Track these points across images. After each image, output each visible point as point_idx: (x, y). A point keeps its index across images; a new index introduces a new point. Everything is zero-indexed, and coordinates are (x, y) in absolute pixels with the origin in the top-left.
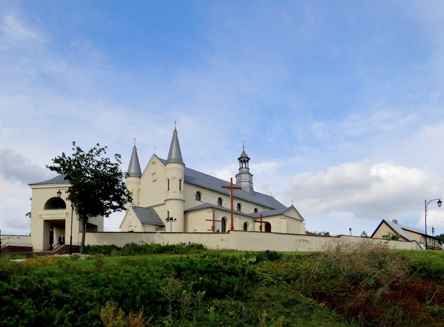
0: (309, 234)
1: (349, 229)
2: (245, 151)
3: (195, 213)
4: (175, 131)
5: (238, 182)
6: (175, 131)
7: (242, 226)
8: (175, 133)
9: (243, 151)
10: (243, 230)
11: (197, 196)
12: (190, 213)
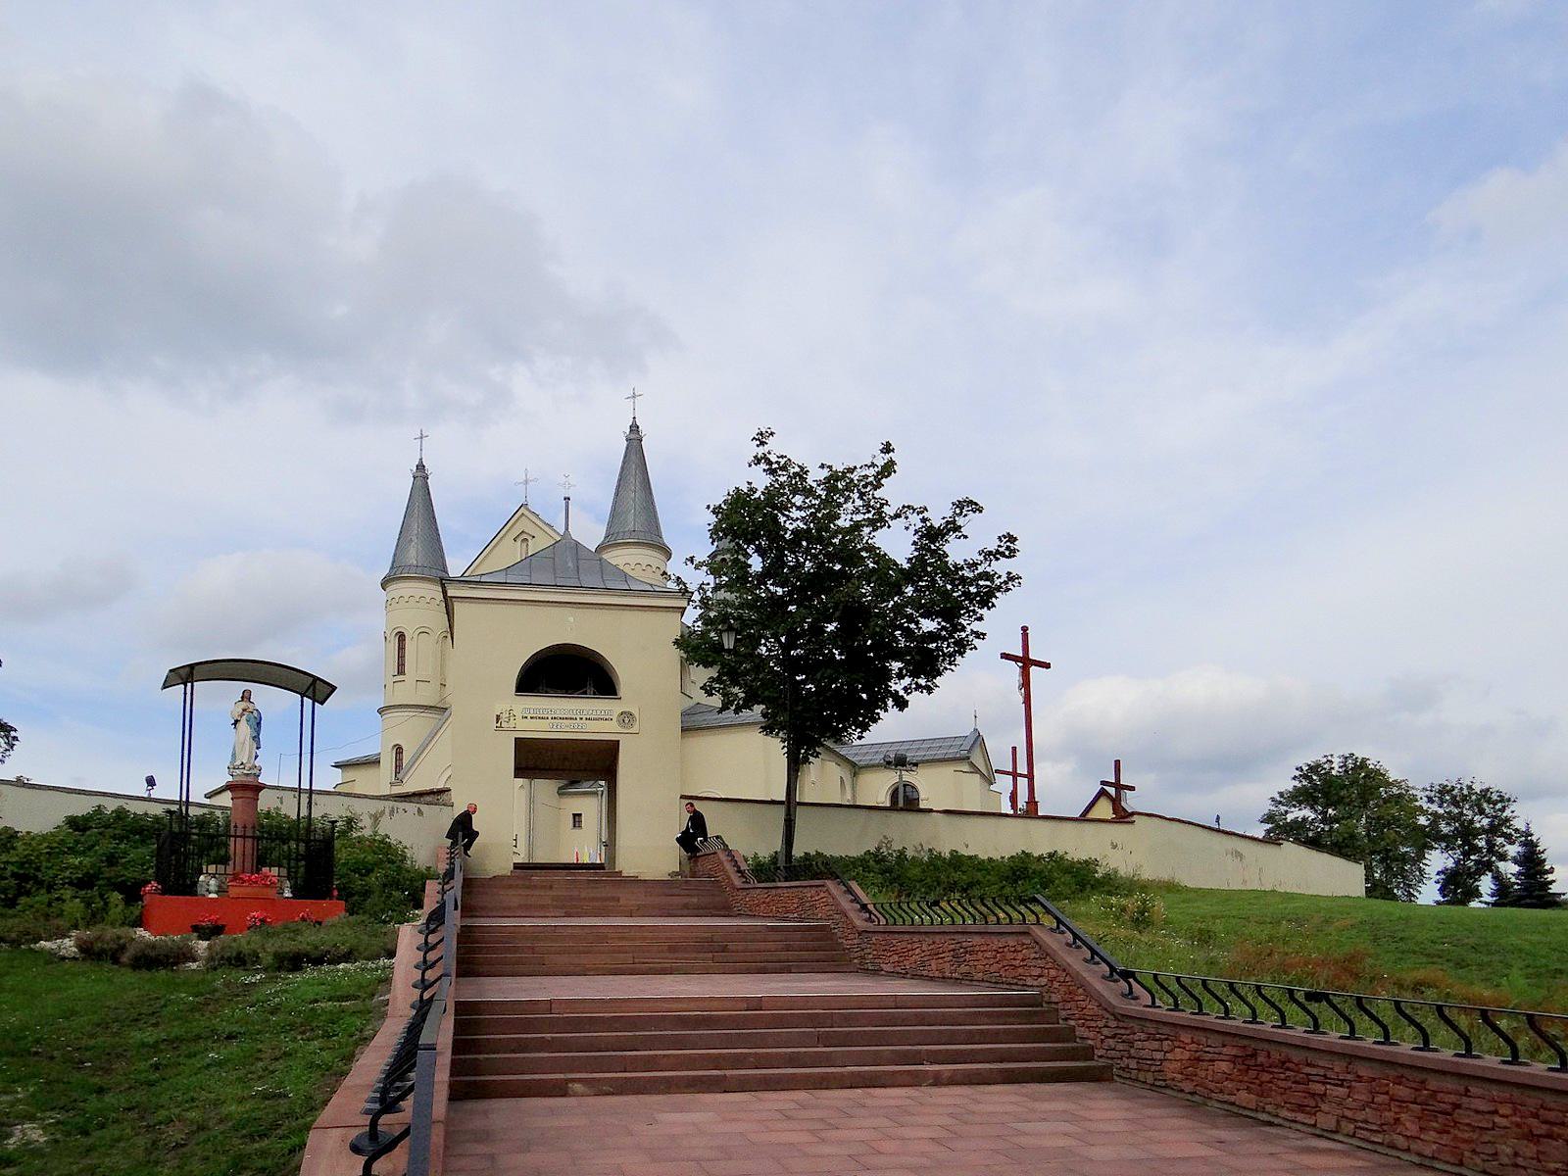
3: (724, 733)
8: (633, 436)
12: (693, 737)
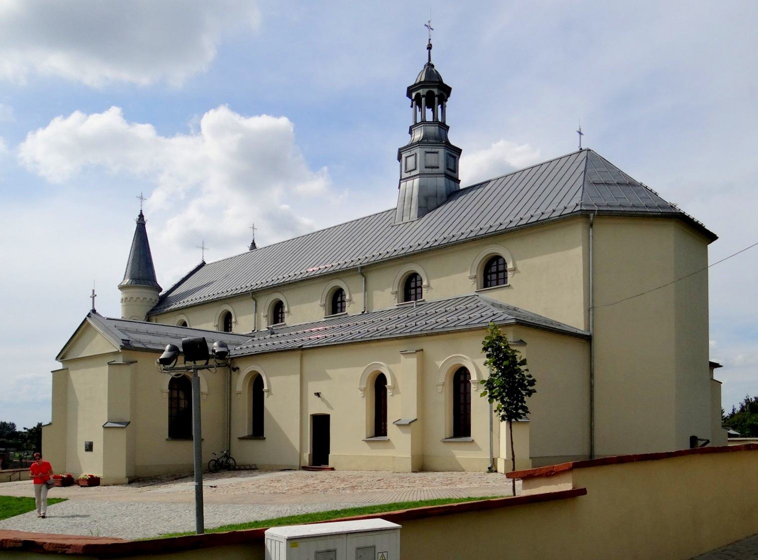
0: (483, 322)
2: (432, 62)
4: (141, 216)
5: (405, 175)
6: (141, 216)
10: (98, 334)
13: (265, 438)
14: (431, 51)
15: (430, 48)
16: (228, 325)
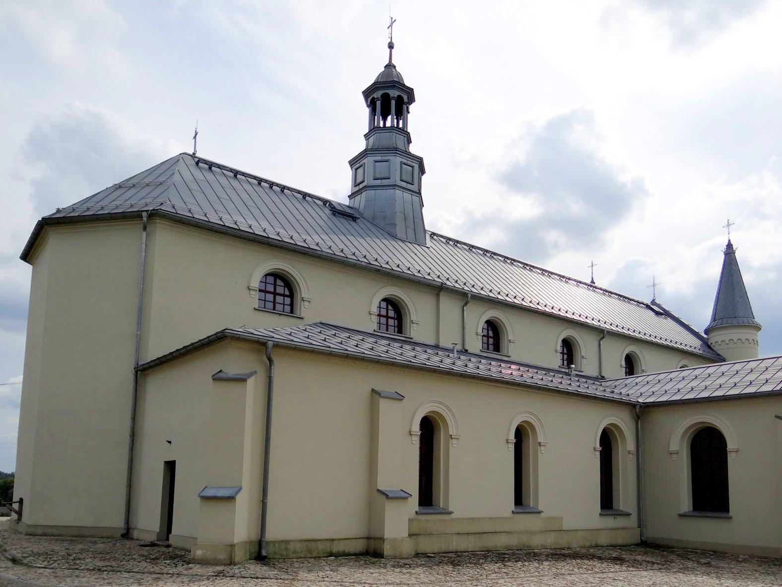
1: (593, 448)
2: (394, 62)
7: (595, 449)
9: (387, 62)
11: (387, 317)
13: (730, 518)
14: (393, 50)
15: (391, 46)
16: (629, 370)
